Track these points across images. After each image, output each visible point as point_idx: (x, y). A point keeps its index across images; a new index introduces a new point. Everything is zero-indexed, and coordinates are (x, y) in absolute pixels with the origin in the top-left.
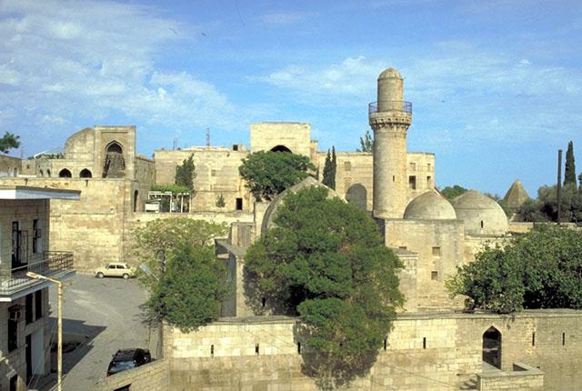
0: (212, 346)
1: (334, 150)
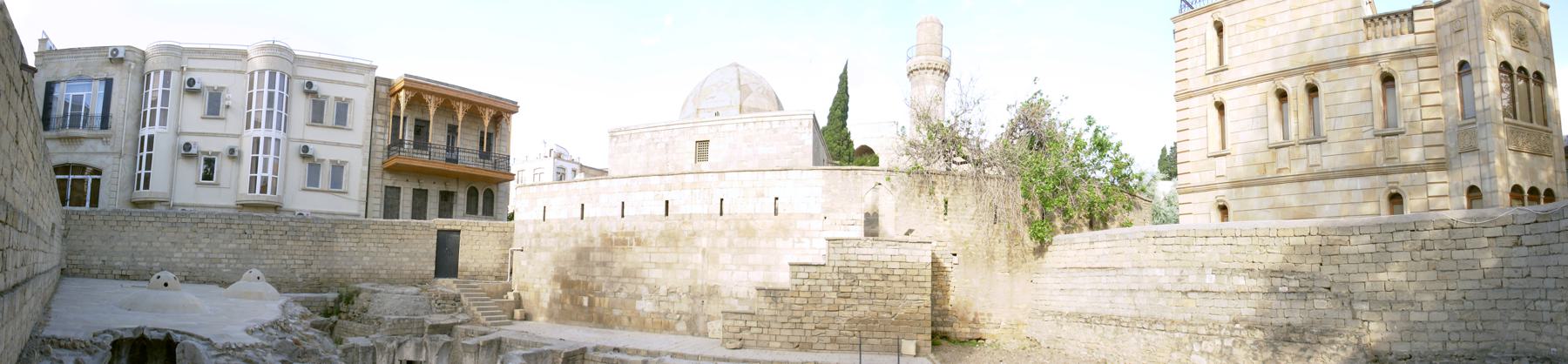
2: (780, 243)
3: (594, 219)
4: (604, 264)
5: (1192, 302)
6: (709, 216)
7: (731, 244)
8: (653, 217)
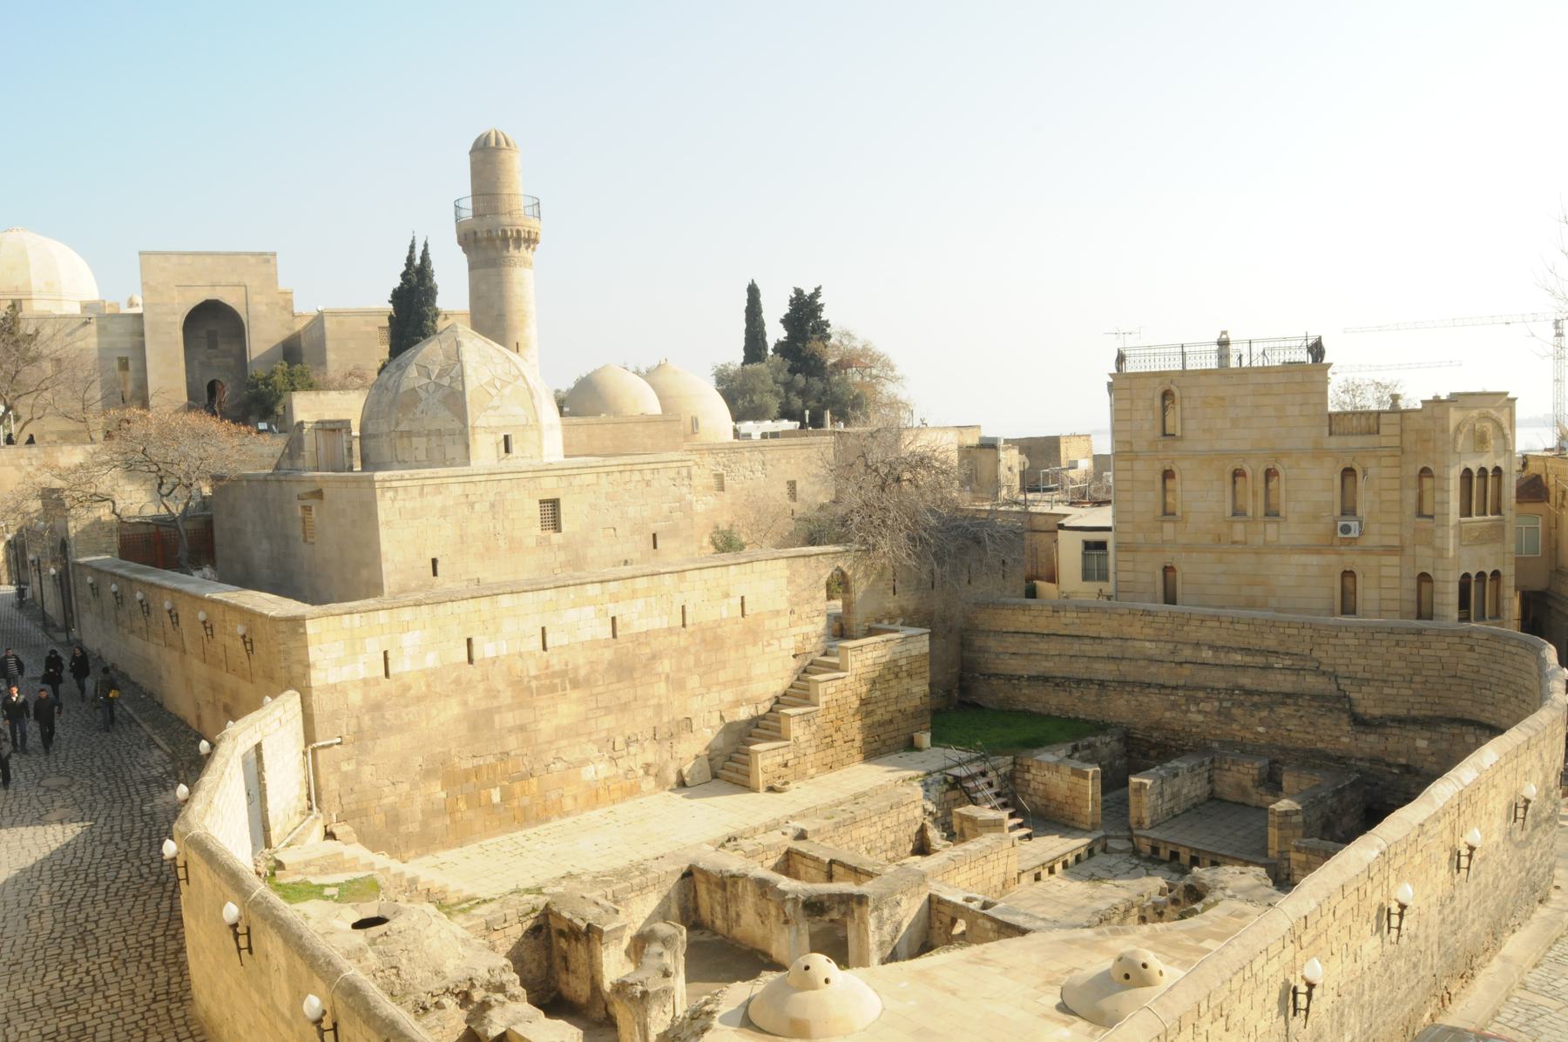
0: (385, 653)
1: (426, 245)
2: (750, 651)
3: (494, 661)
4: (522, 728)
5: (1186, 670)
6: (670, 630)
7: (697, 663)
8: (594, 644)
